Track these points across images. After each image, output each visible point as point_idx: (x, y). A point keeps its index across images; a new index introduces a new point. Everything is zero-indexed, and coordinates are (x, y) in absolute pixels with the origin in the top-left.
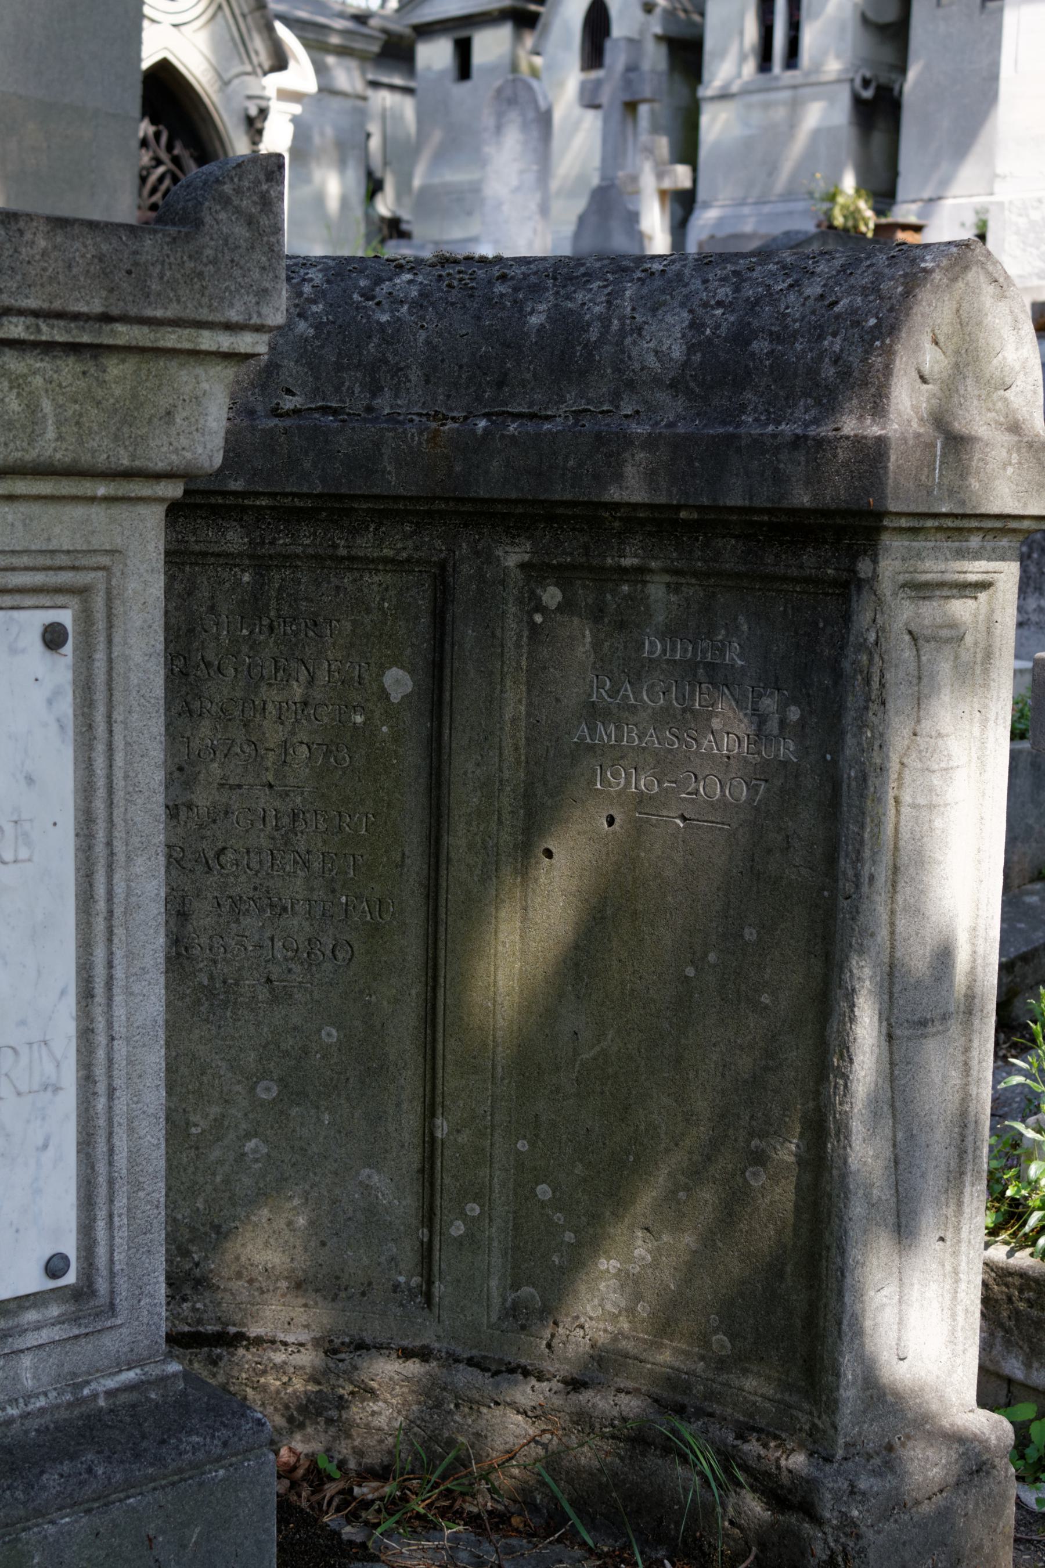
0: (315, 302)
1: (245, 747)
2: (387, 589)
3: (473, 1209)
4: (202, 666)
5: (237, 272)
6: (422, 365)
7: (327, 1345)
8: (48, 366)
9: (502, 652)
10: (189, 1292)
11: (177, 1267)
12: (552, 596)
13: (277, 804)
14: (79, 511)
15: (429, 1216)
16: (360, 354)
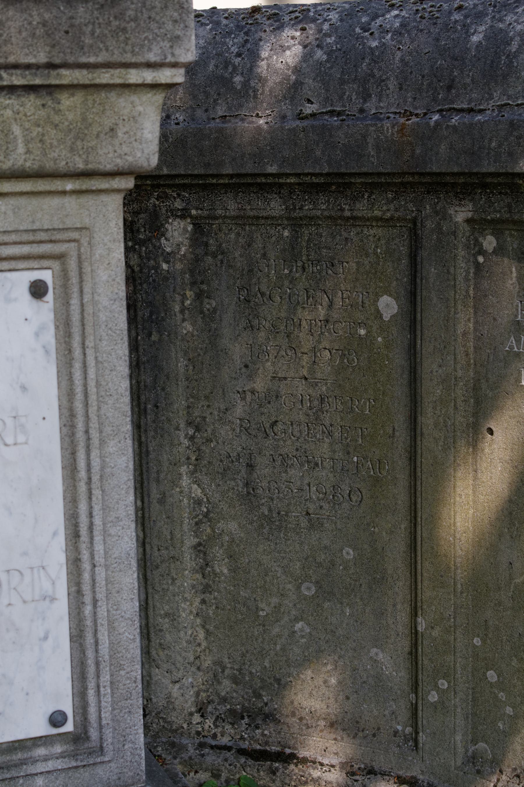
0: (330, 36)
1: (288, 351)
2: (379, 240)
3: (443, 684)
4: (259, 295)
5: (153, 26)
6: (397, 77)
7: (348, 768)
8: (15, 102)
9: (455, 285)
10: (260, 722)
11: (253, 705)
12: (489, 242)
13: (310, 391)
14: (56, 201)
15: (415, 686)
16: (356, 71)
